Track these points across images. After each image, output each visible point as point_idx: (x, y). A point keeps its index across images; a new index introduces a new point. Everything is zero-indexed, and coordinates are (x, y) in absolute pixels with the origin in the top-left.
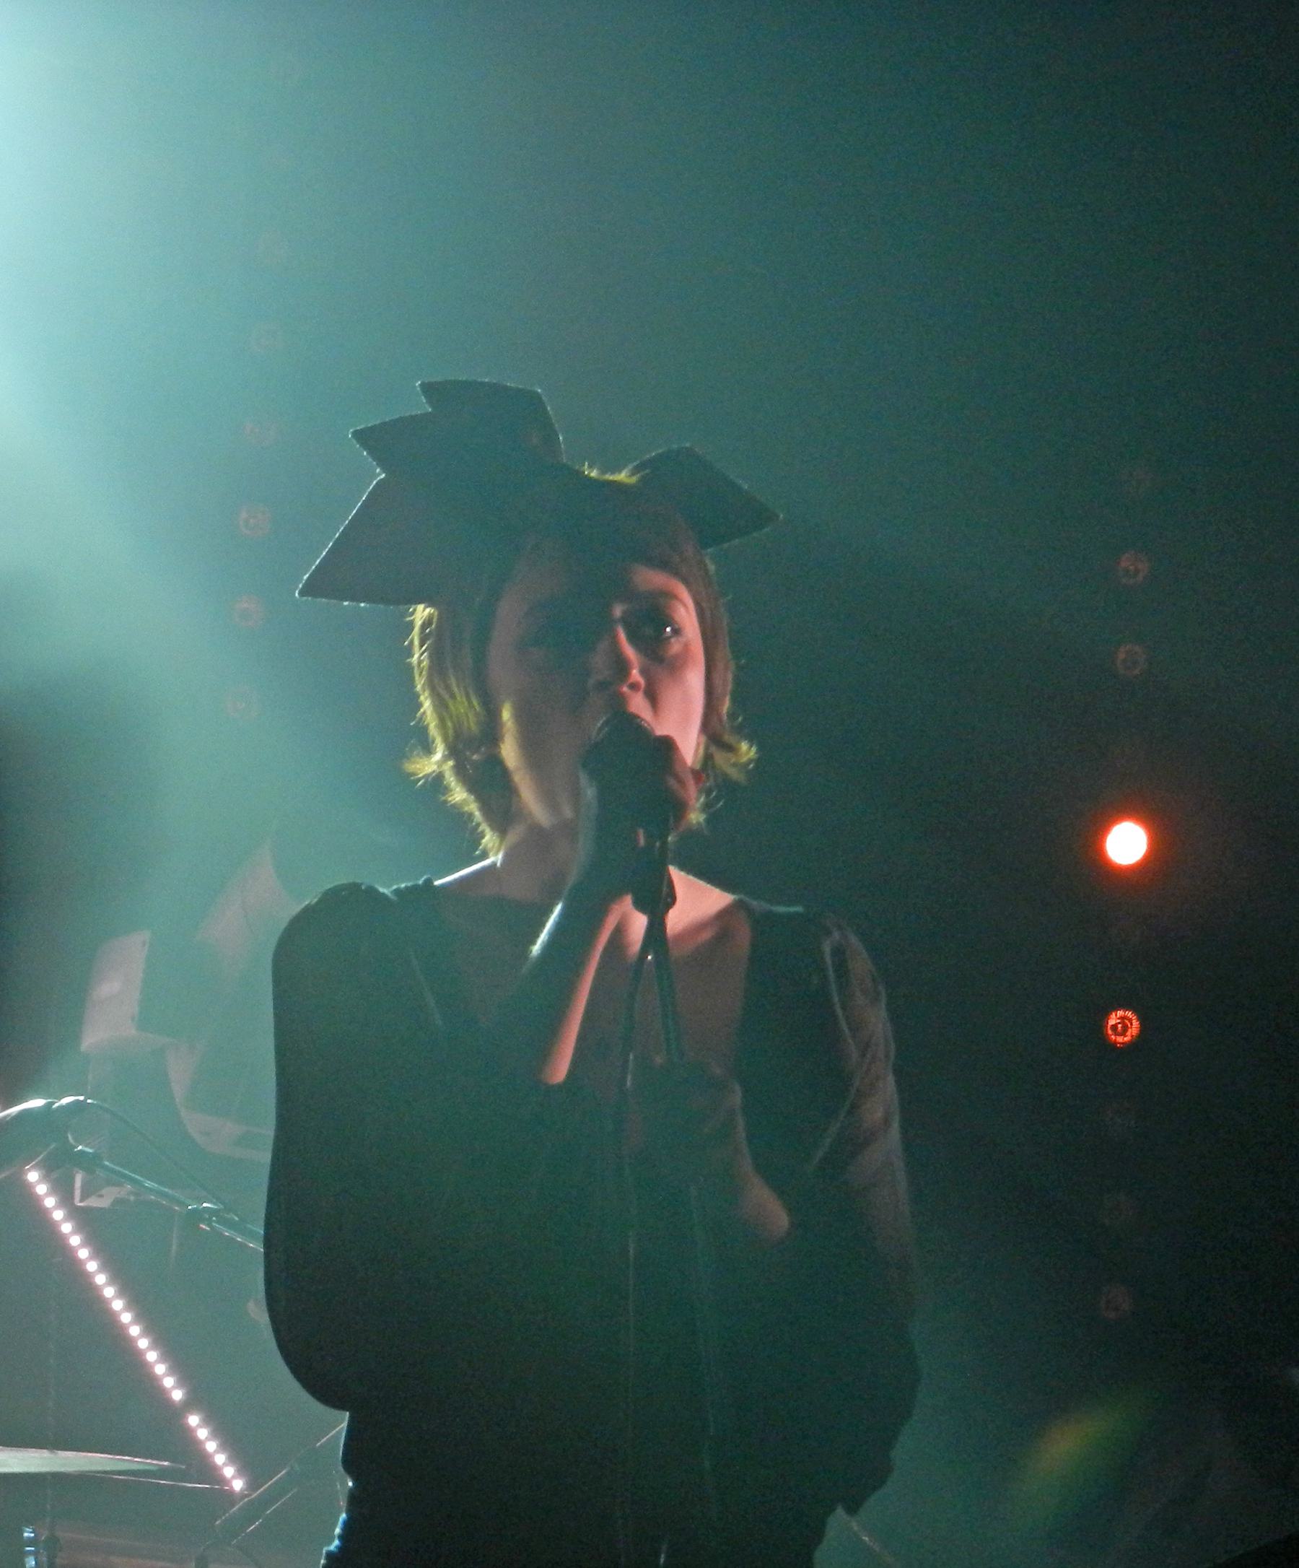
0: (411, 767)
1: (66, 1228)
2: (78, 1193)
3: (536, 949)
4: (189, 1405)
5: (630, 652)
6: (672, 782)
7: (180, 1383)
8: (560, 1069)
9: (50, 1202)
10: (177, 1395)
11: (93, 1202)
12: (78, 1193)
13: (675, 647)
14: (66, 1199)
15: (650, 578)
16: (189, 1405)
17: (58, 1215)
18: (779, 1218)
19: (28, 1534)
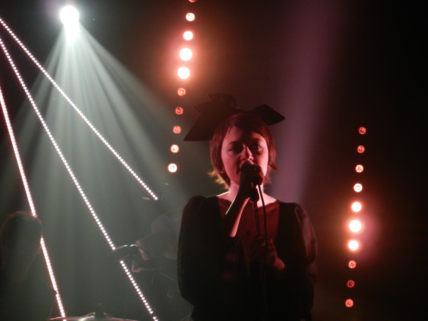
0: (209, 174)
1: (130, 276)
2: (133, 269)
3: (42, 242)
4: (153, 315)
5: (249, 151)
6: (260, 174)
7: (156, 196)
8: (234, 233)
9: (127, 271)
10: (151, 312)
11: (136, 271)
12: (133, 269)
13: (260, 149)
14: (130, 271)
15: (256, 135)
16: (153, 315)
17: (128, 273)
18: (283, 265)
19: (173, 168)
